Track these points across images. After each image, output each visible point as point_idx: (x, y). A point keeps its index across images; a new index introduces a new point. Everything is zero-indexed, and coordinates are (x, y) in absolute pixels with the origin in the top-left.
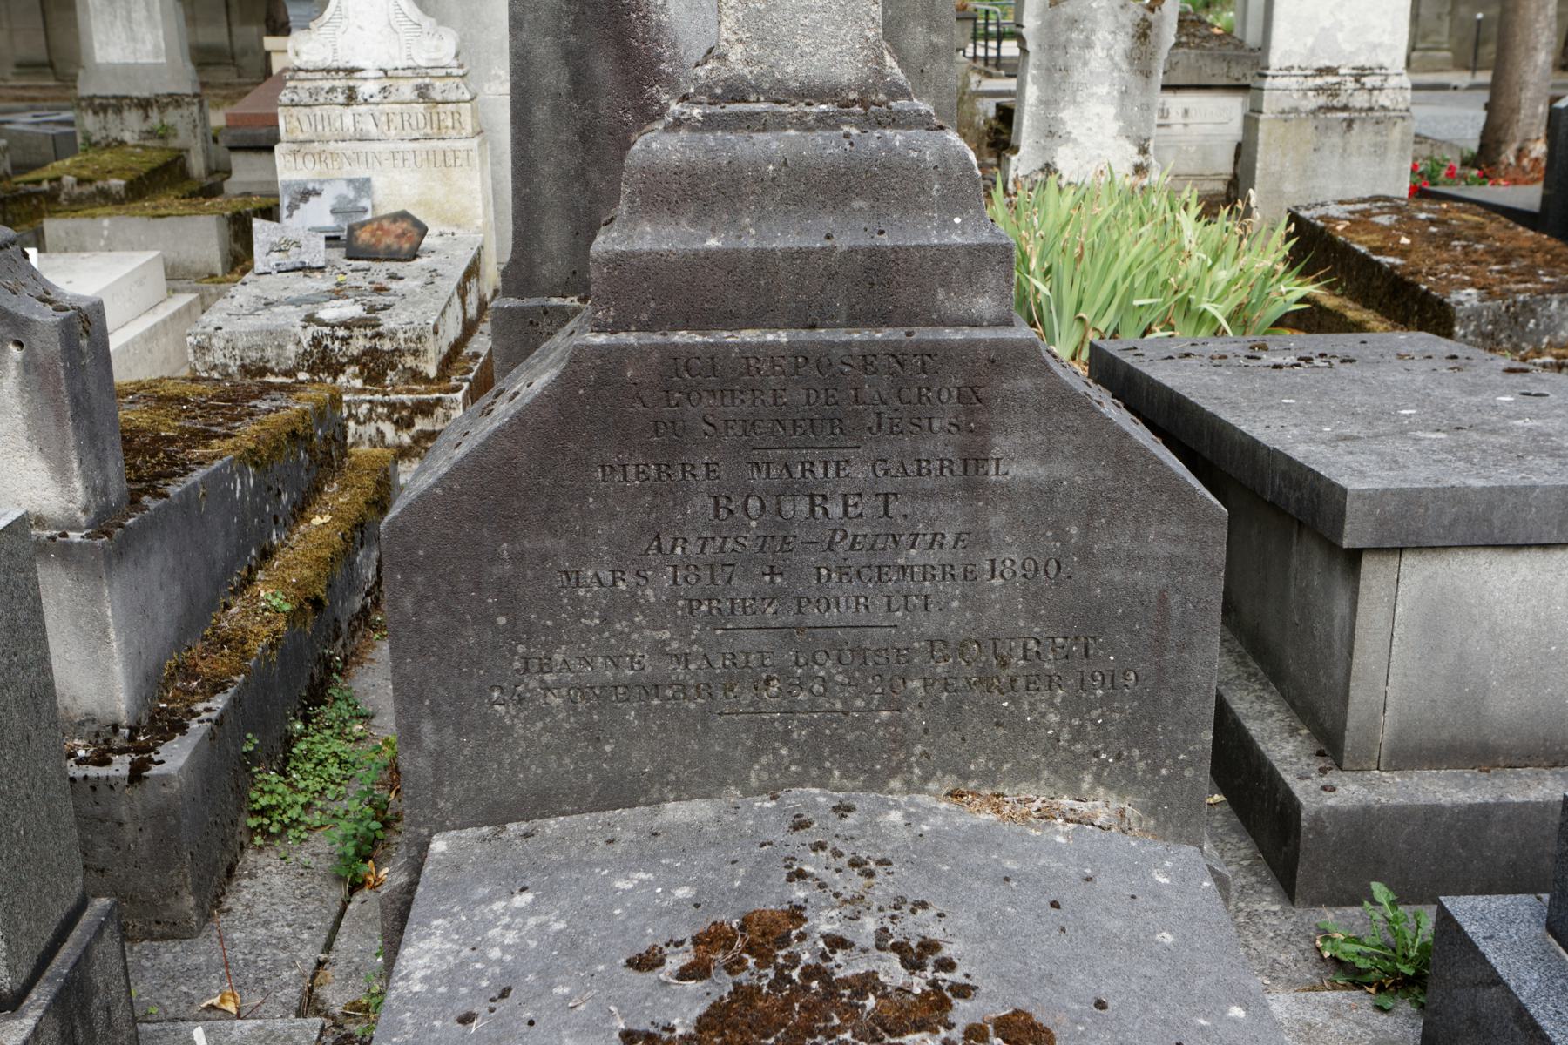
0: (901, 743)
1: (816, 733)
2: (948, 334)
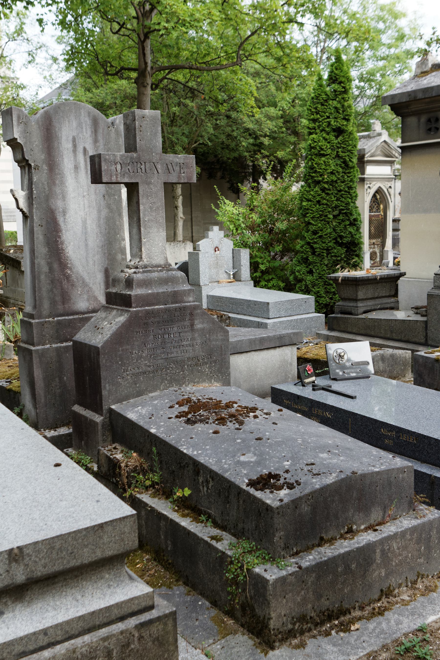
0: (184, 378)
1: (171, 378)
2: (186, 304)
